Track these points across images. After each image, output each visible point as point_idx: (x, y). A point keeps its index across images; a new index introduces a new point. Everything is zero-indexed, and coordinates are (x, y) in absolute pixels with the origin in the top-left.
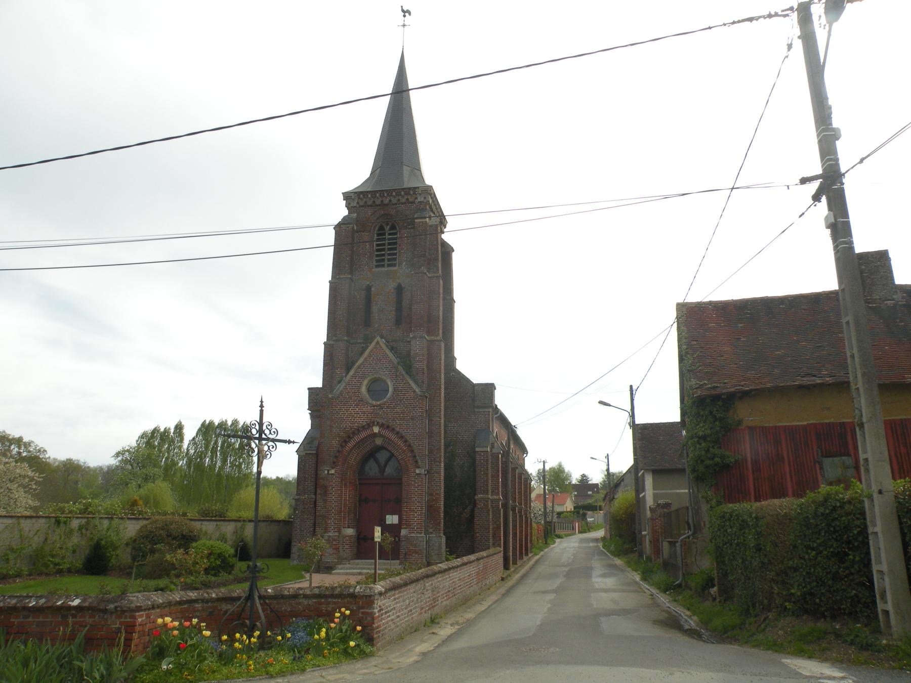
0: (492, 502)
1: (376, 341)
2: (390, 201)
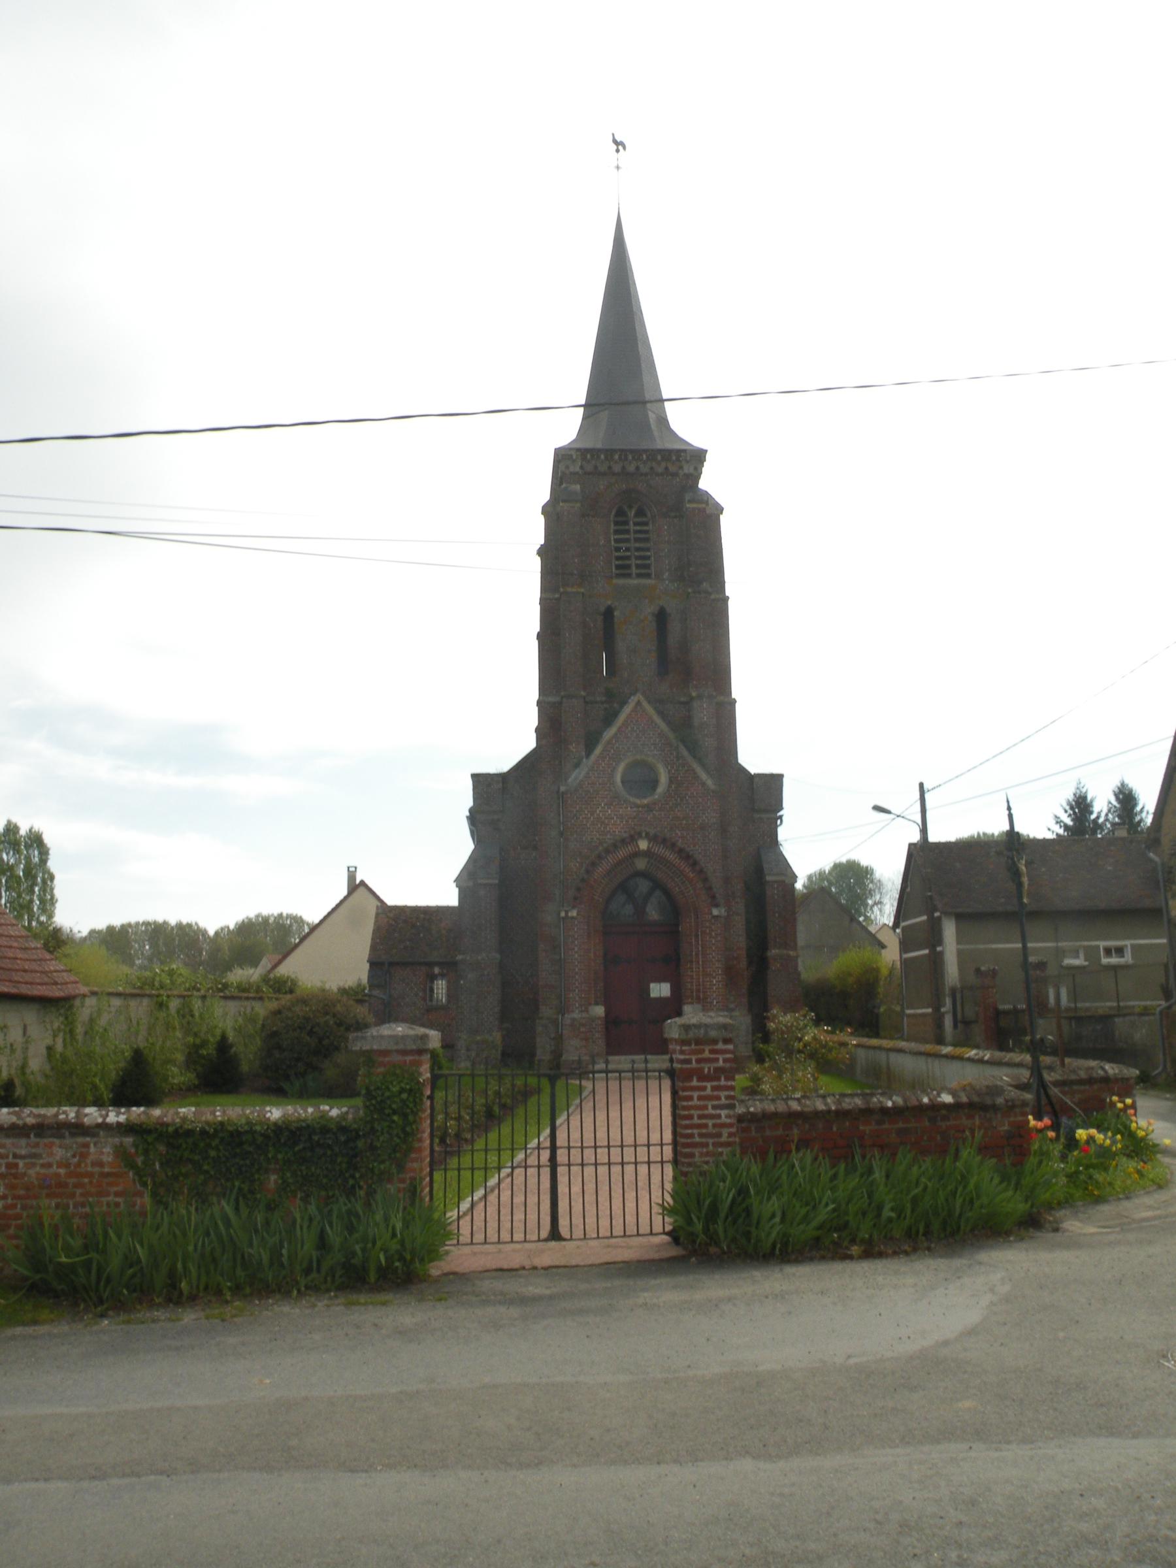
2: (637, 468)
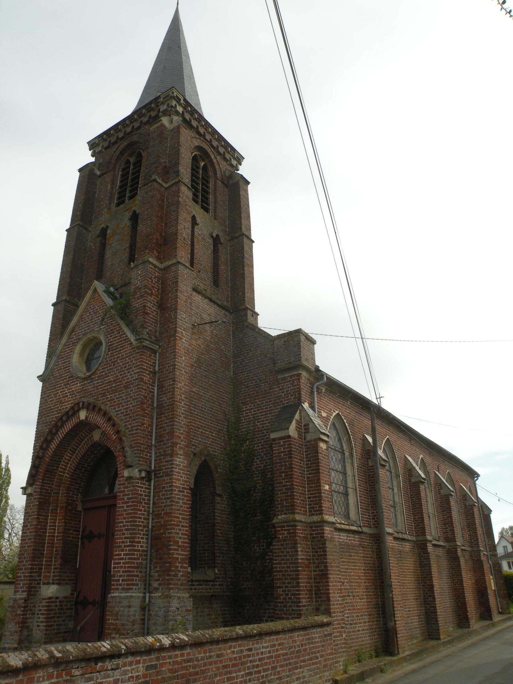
0: (311, 527)
1: (92, 288)
